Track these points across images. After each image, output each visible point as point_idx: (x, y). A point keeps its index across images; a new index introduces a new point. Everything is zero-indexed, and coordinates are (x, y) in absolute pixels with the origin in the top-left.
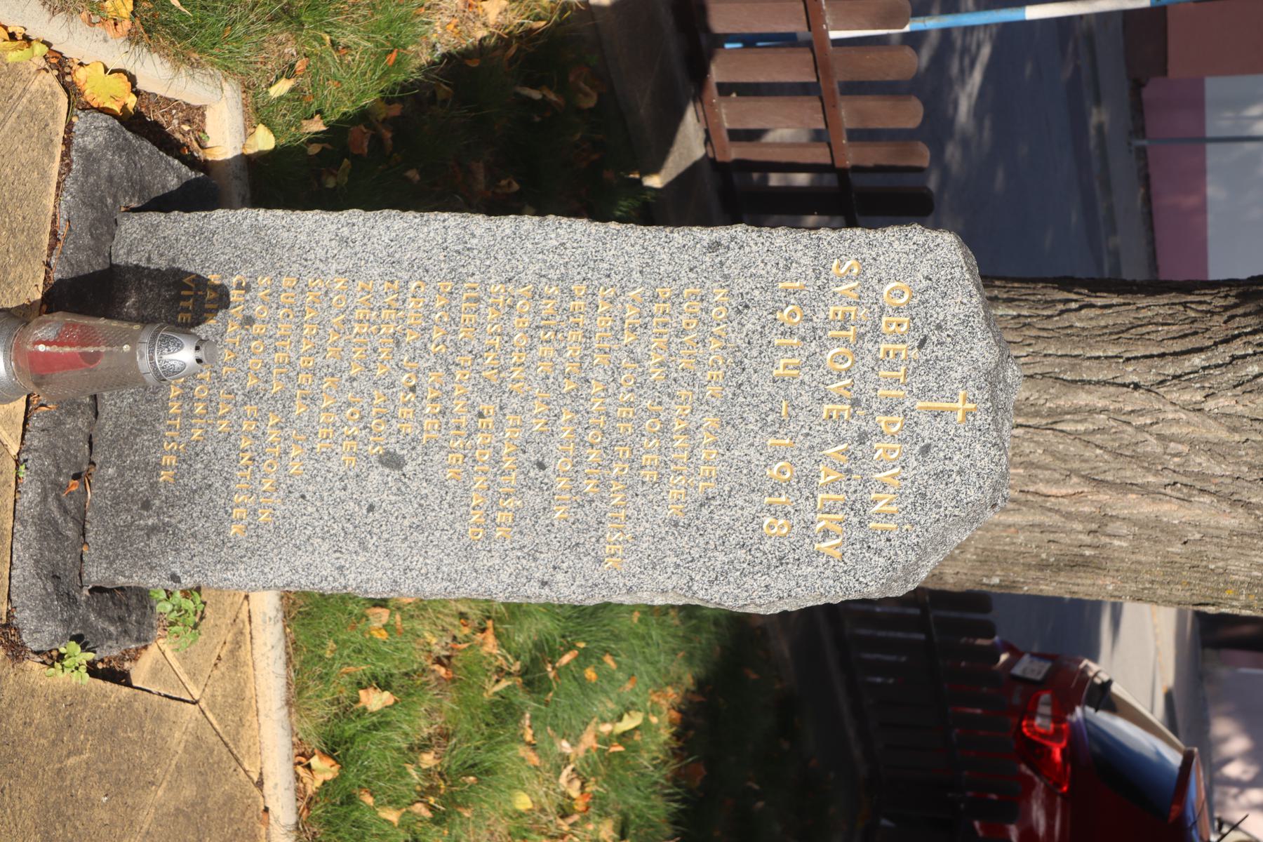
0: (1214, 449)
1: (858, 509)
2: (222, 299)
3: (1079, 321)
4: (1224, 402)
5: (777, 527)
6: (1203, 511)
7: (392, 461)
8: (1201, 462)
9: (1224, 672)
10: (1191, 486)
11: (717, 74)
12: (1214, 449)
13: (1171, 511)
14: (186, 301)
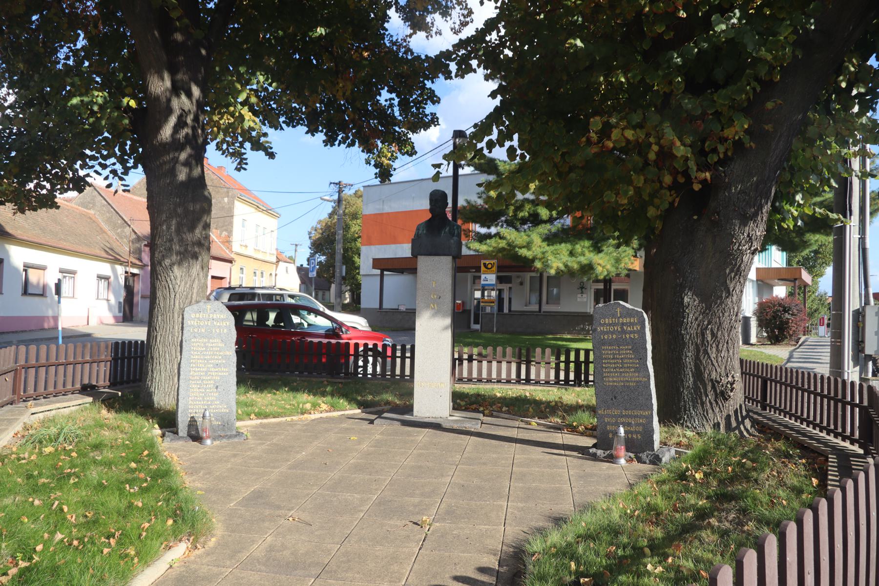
0: (186, 284)
1: (223, 320)
2: (192, 417)
3: (162, 305)
4: (178, 282)
5: (225, 331)
6: (195, 286)
7: (217, 387)
8: (188, 286)
9: (140, 315)
10: (191, 286)
11: (94, 383)
12: (186, 284)
13: (195, 291)
14: (192, 424)
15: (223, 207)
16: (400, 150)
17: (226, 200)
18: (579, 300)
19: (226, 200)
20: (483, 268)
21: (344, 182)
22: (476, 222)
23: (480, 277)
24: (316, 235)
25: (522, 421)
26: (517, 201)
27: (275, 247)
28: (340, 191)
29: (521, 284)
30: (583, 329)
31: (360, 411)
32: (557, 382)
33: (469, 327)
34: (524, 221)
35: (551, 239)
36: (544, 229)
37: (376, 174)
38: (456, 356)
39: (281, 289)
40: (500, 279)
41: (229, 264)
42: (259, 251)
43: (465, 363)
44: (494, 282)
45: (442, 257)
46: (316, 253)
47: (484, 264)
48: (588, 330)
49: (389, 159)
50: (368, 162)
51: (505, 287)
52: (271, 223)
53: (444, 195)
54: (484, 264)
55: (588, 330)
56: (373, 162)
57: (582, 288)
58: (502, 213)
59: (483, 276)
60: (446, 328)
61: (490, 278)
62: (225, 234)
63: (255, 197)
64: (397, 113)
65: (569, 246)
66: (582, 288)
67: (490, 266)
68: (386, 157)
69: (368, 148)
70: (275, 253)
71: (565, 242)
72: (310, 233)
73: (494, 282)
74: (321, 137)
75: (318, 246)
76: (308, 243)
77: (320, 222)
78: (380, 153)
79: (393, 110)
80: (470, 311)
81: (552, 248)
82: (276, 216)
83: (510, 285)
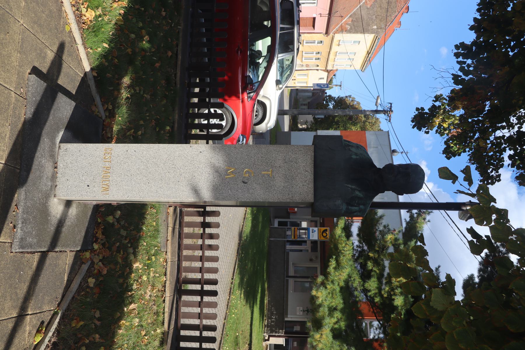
15: (369, 25)
16: (452, 138)
17: (375, 27)
18: (298, 308)
19: (375, 27)
20: (323, 229)
21: (393, 115)
22: (362, 223)
23: (316, 226)
24: (348, 101)
25: (55, 314)
26: (382, 260)
27: (339, 68)
28: (384, 112)
29: (311, 260)
30: (272, 314)
31: (88, 69)
32: (178, 327)
33: (276, 217)
34: (363, 266)
35: (347, 290)
36: (357, 282)
37: (423, 109)
38: (208, 209)
39: (298, 49)
40: (314, 242)
41: (324, 32)
42: (336, 55)
43: (200, 219)
44: (311, 238)
45: (311, 185)
46: (335, 101)
47: (326, 230)
48: (271, 318)
49: (440, 126)
50: (438, 98)
51: (308, 246)
52: (358, 66)
53: (415, 187)
54: (326, 230)
55: (271, 318)
56: (437, 104)
57: (308, 311)
58: (371, 247)
59: (316, 229)
60: (196, 191)
61: (314, 236)
62: (348, 27)
63: (377, 52)
64: (499, 133)
65: (340, 306)
66: (308, 311)
67: (324, 234)
68: (443, 121)
69: (454, 99)
70: (335, 69)
71: (344, 303)
72: (350, 96)
73: (311, 238)
74: (470, 37)
75: (341, 103)
76: (343, 95)
77: (359, 103)
78: (447, 115)
79: (503, 128)
80: (289, 218)
81: (338, 289)
82: (363, 67)
83: (310, 251)
